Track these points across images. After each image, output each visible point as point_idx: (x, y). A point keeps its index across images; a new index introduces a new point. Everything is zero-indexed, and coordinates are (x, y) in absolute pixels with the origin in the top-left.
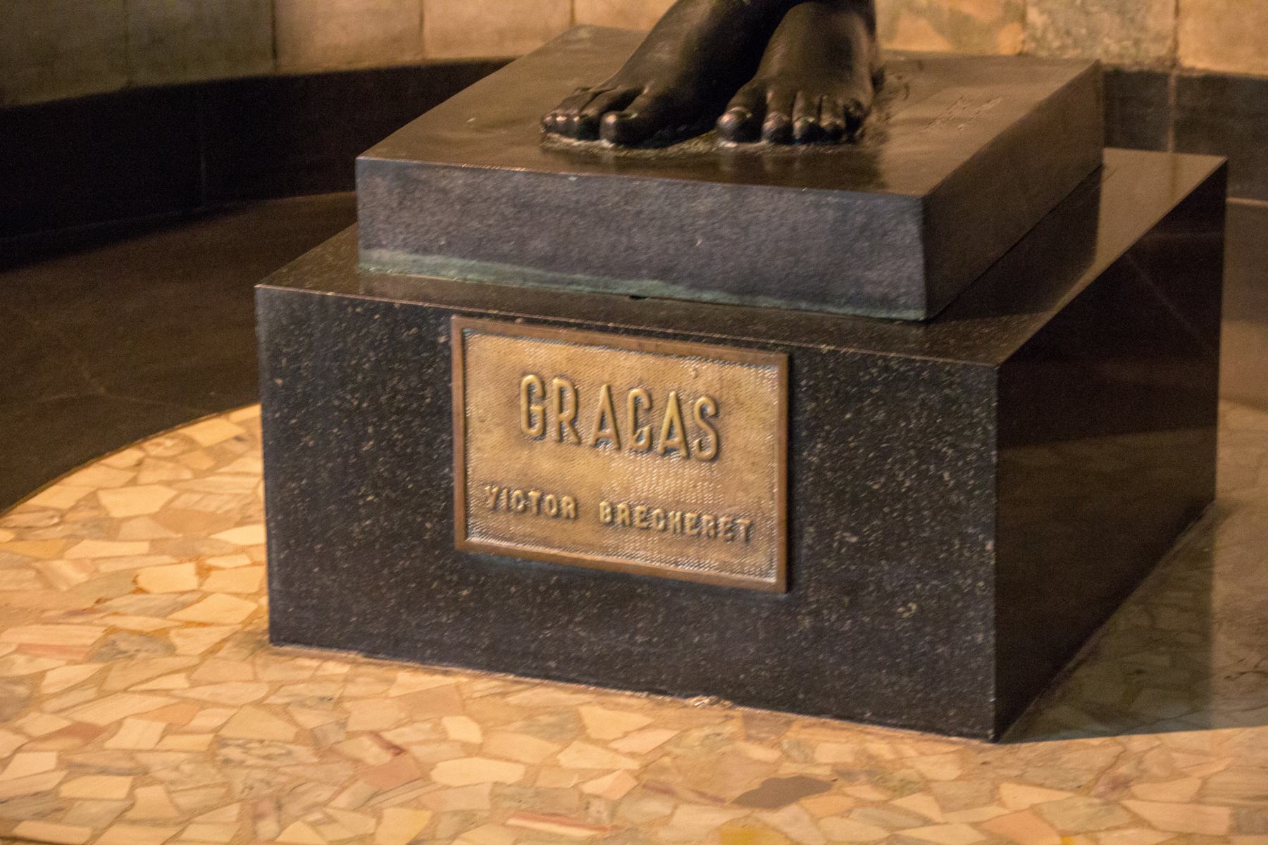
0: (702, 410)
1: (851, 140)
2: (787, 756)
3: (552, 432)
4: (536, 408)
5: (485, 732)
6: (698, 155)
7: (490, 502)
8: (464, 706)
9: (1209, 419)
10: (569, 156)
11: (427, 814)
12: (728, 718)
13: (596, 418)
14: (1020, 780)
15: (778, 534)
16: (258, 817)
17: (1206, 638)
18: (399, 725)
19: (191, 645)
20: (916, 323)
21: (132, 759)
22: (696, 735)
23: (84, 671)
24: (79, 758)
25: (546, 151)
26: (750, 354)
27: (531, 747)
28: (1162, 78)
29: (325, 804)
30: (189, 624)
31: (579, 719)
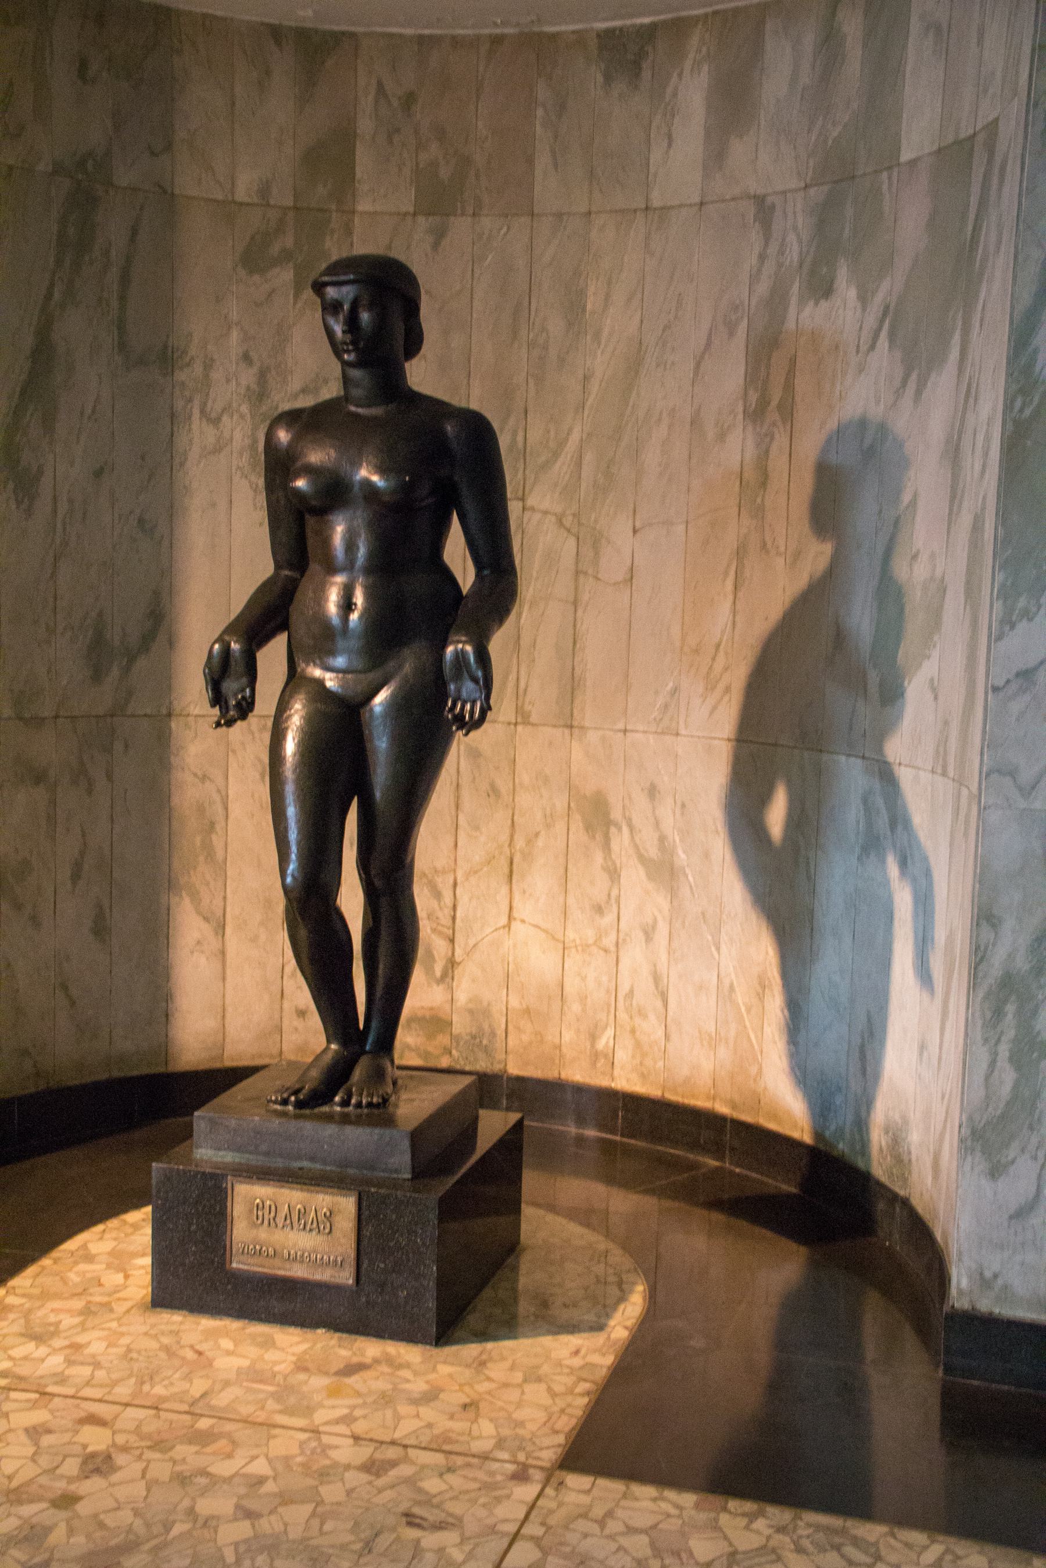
0: (325, 1214)
2: (355, 1354)
3: (266, 1222)
4: (260, 1213)
5: (235, 1346)
6: (326, 1113)
7: (241, 1250)
8: (227, 1333)
9: (517, 1211)
10: (275, 1111)
11: (210, 1382)
12: (331, 1338)
13: (283, 1217)
14: (445, 1362)
15: (353, 1263)
16: (143, 1383)
17: (516, 1300)
18: (201, 1342)
19: (120, 1308)
20: (408, 1180)
22: (319, 1346)
23: (77, 1320)
24: (73, 1358)
25: (268, 1111)
26: (344, 1192)
27: (253, 1351)
28: (502, 1077)
29: (169, 1378)
30: (119, 1299)
31: (273, 1339)
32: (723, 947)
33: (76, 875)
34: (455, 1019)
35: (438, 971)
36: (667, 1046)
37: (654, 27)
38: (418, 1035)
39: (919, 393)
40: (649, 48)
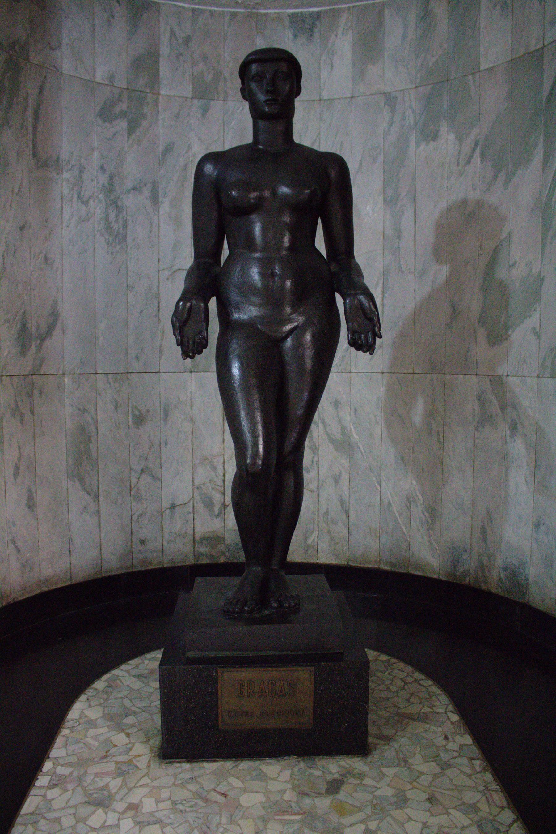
1: (170, 540)
21: (154, 816)
32: (383, 483)
33: (16, 473)
34: (227, 535)
35: (216, 509)
36: (350, 538)
37: (319, 13)
38: (207, 547)
39: (508, 181)
40: (317, 23)
